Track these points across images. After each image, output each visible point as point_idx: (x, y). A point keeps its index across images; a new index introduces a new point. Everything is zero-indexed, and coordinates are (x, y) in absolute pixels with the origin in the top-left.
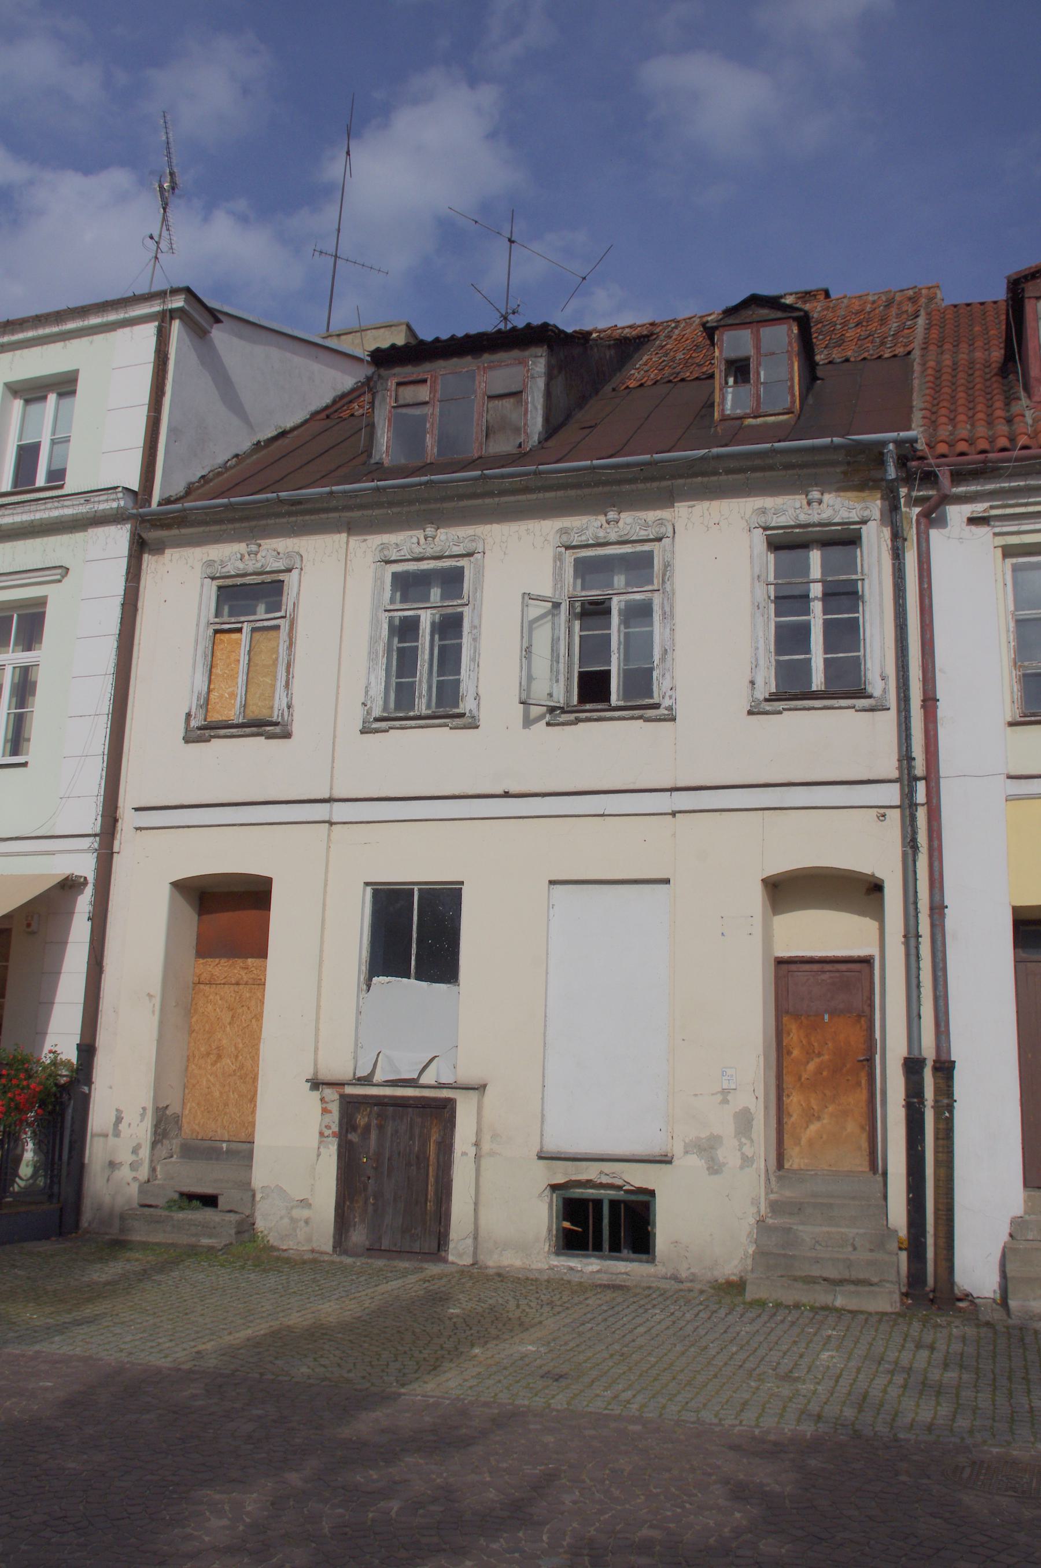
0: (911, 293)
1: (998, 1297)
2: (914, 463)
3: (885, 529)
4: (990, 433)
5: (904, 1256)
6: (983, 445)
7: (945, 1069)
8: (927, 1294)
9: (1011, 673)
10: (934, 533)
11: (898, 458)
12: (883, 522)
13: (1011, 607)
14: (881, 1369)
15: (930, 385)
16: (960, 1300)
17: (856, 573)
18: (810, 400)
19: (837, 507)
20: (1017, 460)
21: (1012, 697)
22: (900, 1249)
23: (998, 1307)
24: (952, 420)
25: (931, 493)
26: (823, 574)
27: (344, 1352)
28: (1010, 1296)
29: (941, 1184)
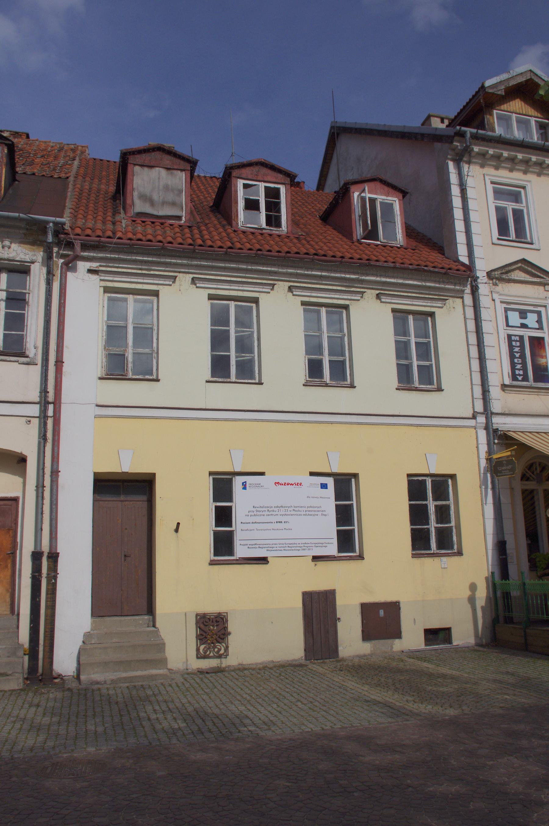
0: (73, 146)
1: (75, 674)
2: (62, 236)
3: (43, 268)
4: (104, 228)
5: (26, 658)
6: (99, 233)
7: (54, 557)
8: (39, 677)
9: (102, 352)
10: (69, 274)
11: (54, 232)
12: (43, 264)
13: (106, 319)
14: (8, 721)
15: (77, 197)
16: (56, 678)
17: (26, 289)
18: (10, 191)
19: (18, 252)
20: (115, 244)
21: (102, 365)
22: (25, 654)
23: (75, 680)
24: (85, 217)
25: (70, 253)
26: (8, 286)
27: (296, 706)
28: (81, 673)
29: (48, 618)
